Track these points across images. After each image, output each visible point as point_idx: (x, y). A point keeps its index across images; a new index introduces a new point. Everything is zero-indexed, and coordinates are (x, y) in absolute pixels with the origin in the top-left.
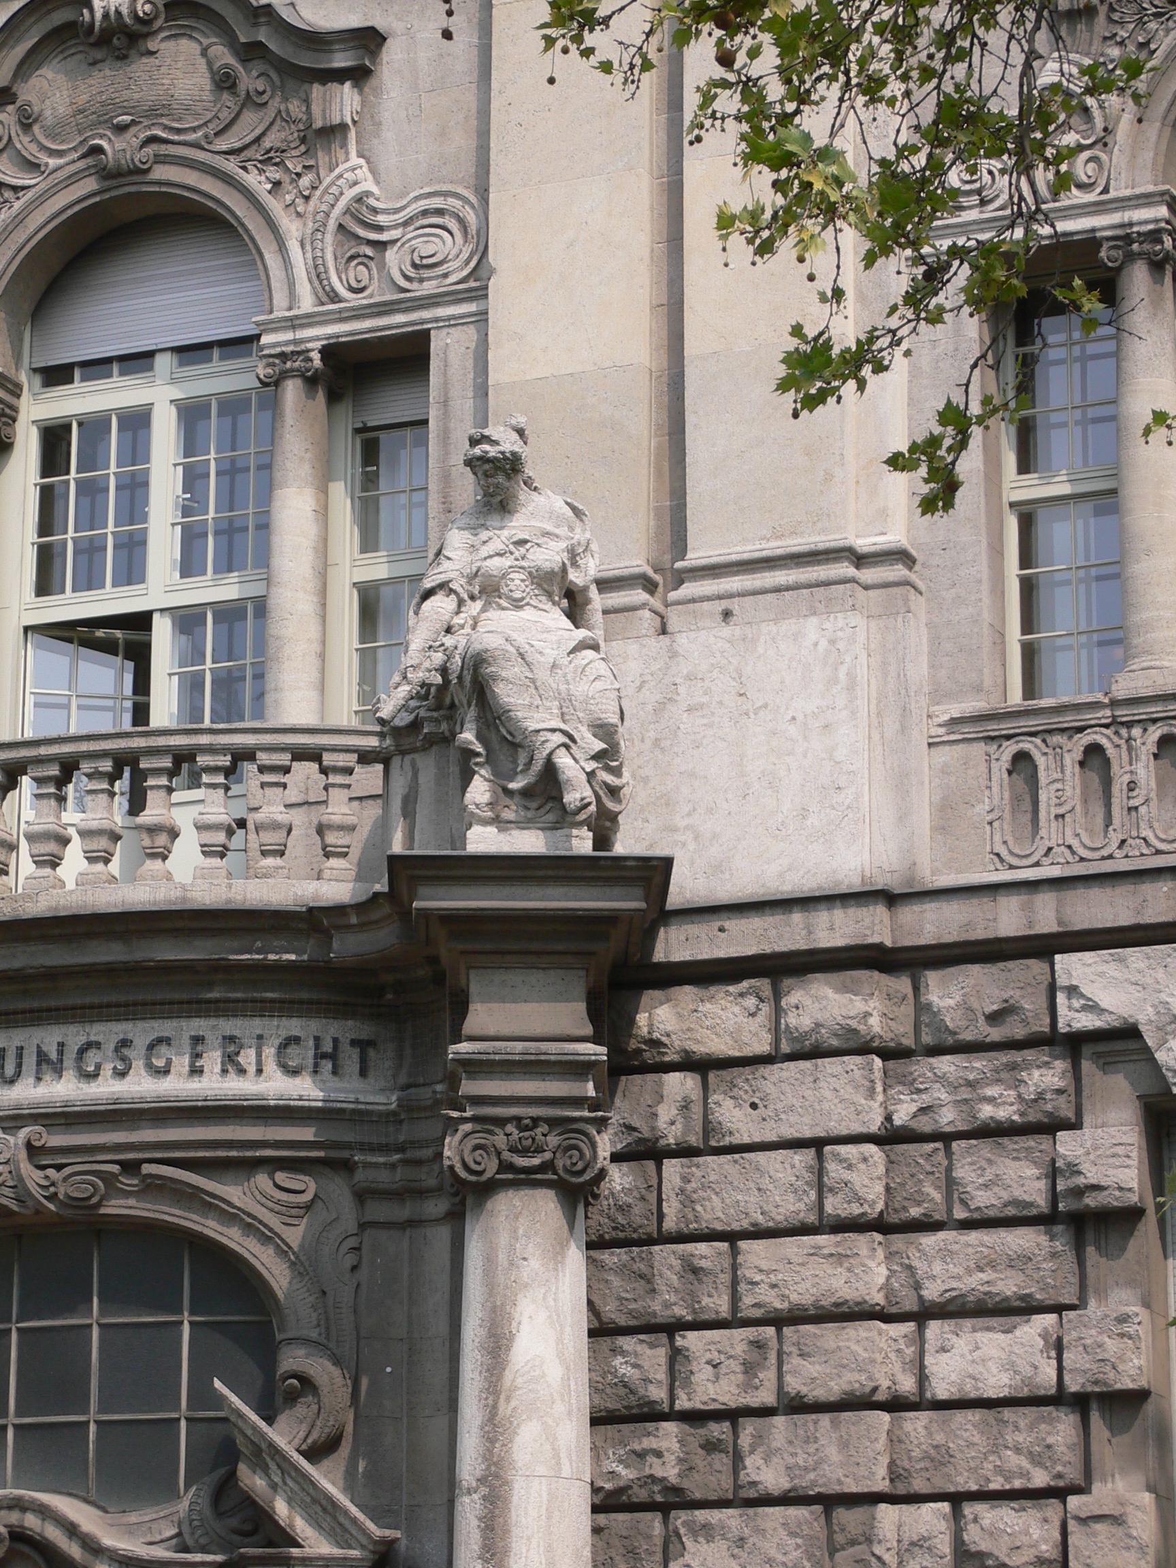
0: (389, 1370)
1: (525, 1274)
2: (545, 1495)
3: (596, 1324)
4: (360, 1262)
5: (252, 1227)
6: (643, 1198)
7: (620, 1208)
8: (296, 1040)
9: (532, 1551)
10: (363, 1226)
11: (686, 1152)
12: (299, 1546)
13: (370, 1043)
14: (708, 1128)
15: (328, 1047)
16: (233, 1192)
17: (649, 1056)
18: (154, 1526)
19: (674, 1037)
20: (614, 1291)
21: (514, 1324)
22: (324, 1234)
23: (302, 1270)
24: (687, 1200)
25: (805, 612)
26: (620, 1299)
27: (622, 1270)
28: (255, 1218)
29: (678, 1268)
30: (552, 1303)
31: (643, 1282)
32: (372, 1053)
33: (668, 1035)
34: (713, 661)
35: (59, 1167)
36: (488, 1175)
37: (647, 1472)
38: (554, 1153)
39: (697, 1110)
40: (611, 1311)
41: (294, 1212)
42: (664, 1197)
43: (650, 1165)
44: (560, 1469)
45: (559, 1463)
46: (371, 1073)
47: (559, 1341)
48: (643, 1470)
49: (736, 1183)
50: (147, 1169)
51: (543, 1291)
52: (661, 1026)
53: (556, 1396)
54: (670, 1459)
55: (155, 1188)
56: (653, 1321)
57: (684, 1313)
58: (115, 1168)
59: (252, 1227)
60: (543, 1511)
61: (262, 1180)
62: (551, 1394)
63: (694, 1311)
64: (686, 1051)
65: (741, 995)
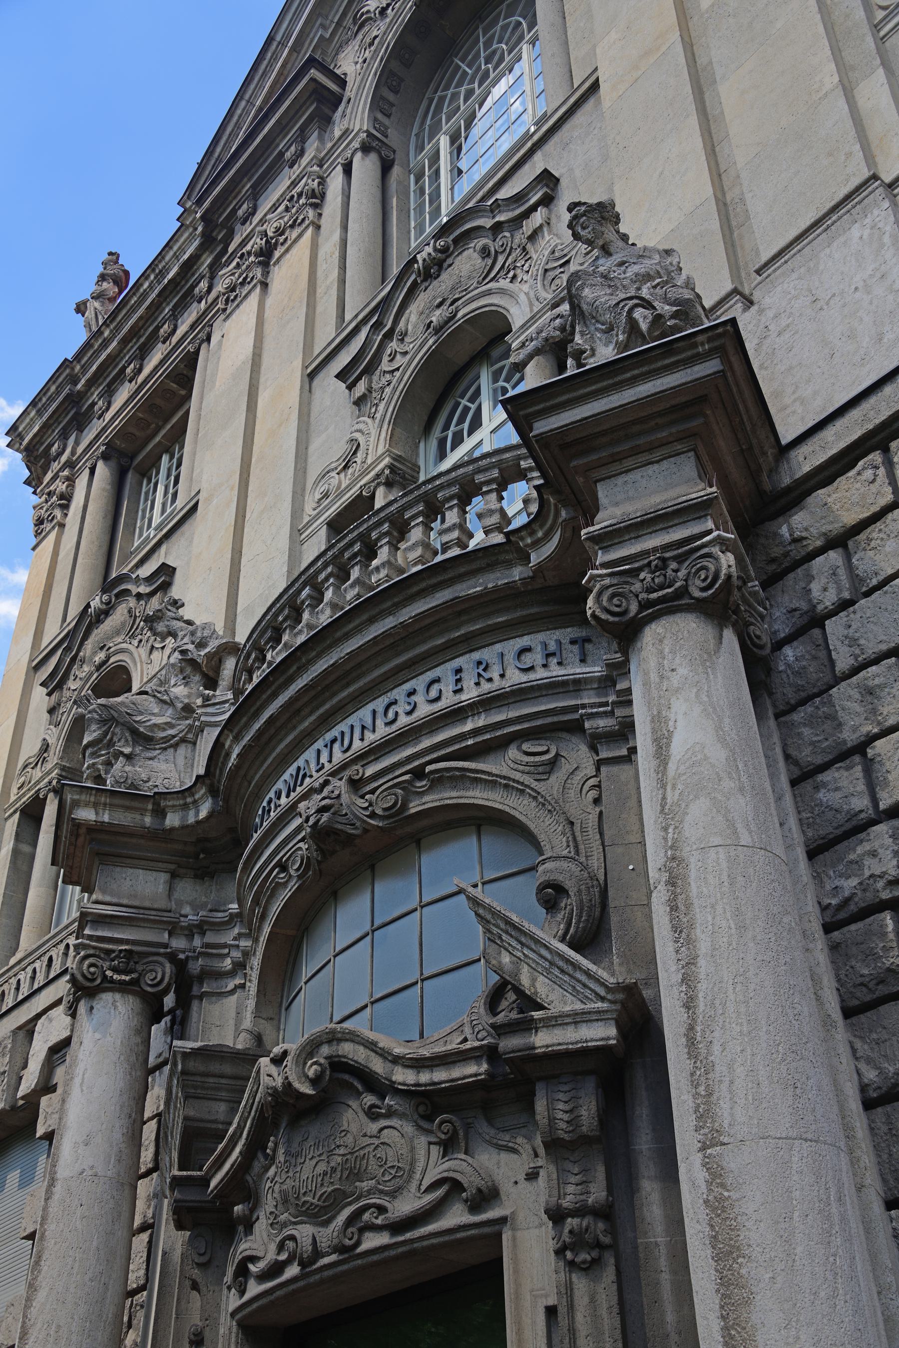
0: (631, 867)
1: (675, 681)
2: (724, 865)
3: (797, 772)
4: (600, 795)
5: (507, 785)
6: (815, 658)
7: (797, 674)
8: (528, 650)
9: (718, 918)
10: (599, 764)
11: (845, 605)
12: (541, 1007)
13: (587, 640)
14: (855, 578)
15: (552, 647)
16: (489, 766)
17: (797, 553)
18: (448, 1038)
19: (812, 529)
20: (806, 739)
21: (671, 723)
22: (569, 781)
23: (550, 808)
24: (853, 642)
25: (848, 226)
26: (813, 743)
27: (809, 722)
28: (509, 779)
29: (857, 696)
30: (706, 699)
31: (829, 722)
32: (588, 646)
33: (806, 529)
34: (789, 296)
35: (372, 792)
36: (632, 614)
37: (867, 873)
38: (686, 580)
39: (842, 573)
40: (807, 756)
41: (541, 769)
42: (831, 647)
43: (816, 632)
44: (738, 838)
45: (735, 832)
46: (589, 659)
47: (719, 728)
48: (863, 874)
49: (890, 608)
50: (428, 769)
51: (695, 690)
52: (800, 526)
53: (723, 775)
54: (888, 855)
55: (439, 781)
56: (845, 748)
57: (870, 728)
58: (407, 777)
59: (507, 785)
60: (725, 877)
61: (513, 752)
62: (717, 773)
63: (879, 723)
64: (825, 534)
65: (859, 474)
